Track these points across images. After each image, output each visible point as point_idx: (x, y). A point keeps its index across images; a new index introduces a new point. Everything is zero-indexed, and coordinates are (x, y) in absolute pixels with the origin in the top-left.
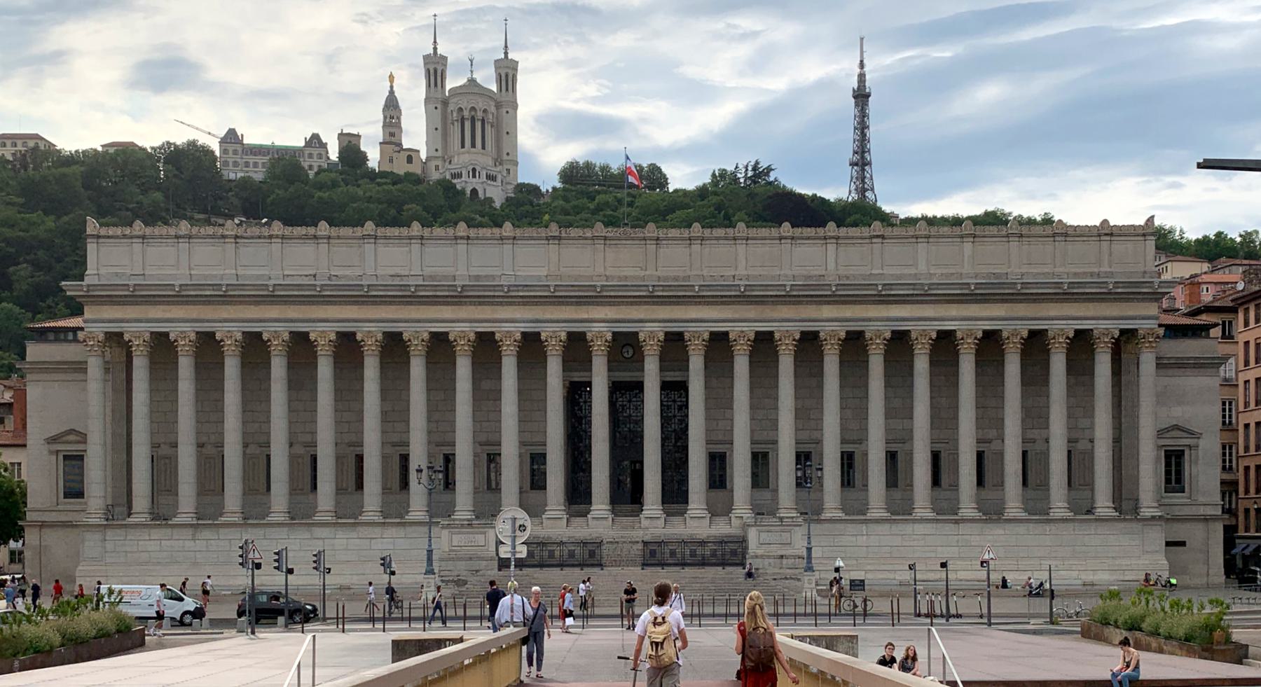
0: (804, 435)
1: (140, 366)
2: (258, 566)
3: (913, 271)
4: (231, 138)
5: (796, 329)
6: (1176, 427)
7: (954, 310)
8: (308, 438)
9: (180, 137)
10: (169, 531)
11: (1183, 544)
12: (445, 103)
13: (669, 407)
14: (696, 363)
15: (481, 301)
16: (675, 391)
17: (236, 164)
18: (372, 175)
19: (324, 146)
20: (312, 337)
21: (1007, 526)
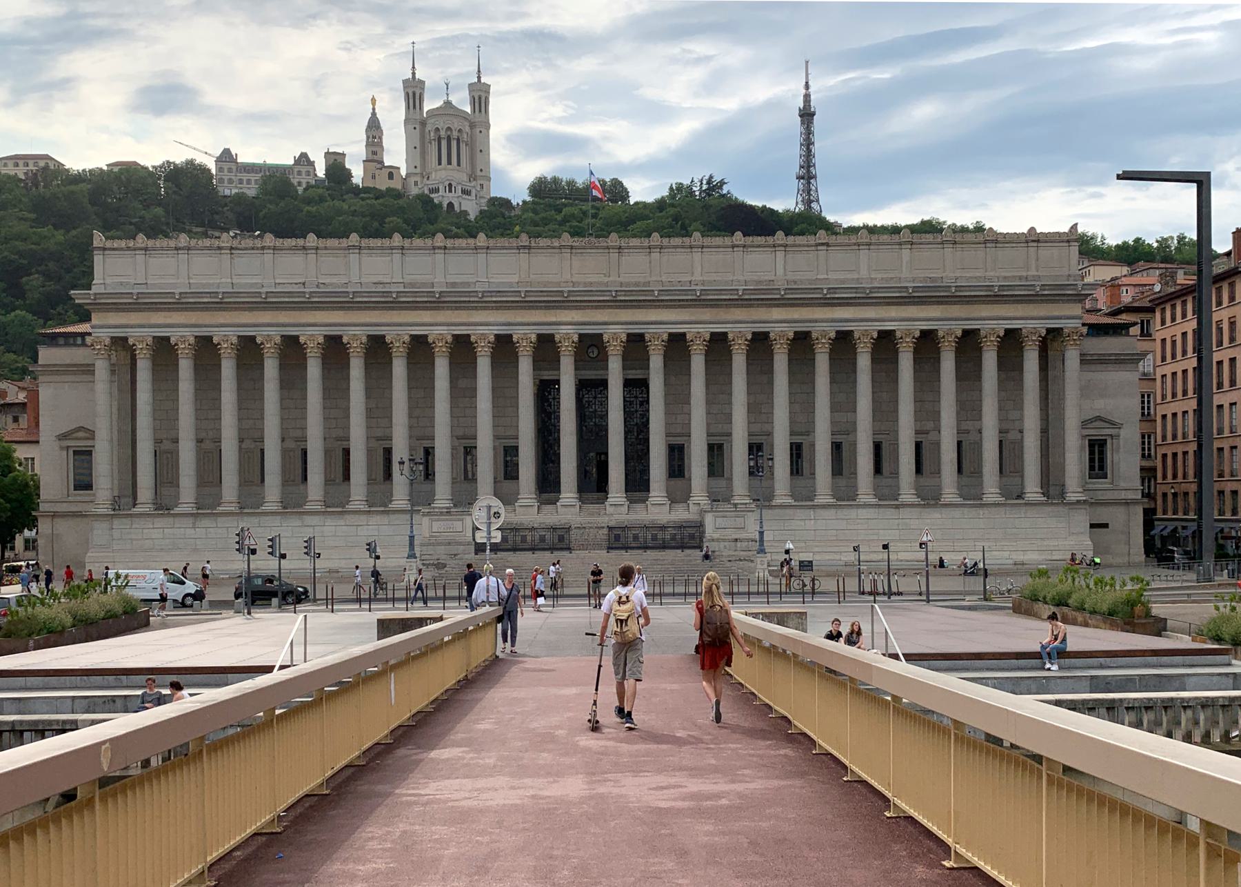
0: (756, 428)
2: (254, 552)
3: (856, 276)
4: (226, 157)
5: (748, 330)
6: (1099, 418)
7: (894, 312)
8: (298, 433)
10: (171, 519)
11: (1106, 526)
12: (423, 123)
13: (631, 403)
14: (656, 362)
15: (458, 306)
16: (637, 388)
17: (230, 181)
18: (356, 191)
19: (312, 164)
21: (944, 510)
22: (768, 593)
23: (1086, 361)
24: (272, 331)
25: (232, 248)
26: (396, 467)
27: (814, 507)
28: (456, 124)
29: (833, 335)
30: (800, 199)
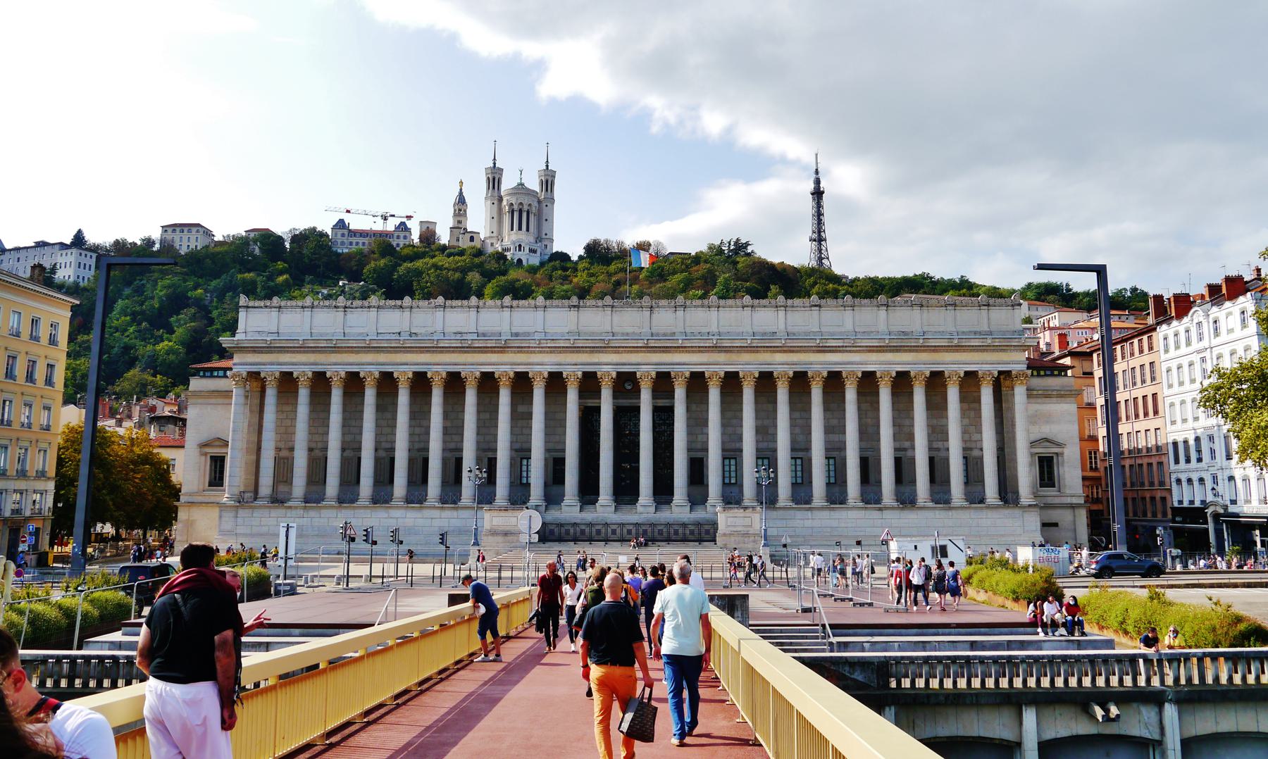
1: (271, 394)
2: (353, 540)
4: (341, 224)
7: (874, 357)
8: (388, 446)
9: (302, 225)
14: (680, 393)
16: (663, 417)
17: (343, 243)
18: (443, 248)
20: (395, 375)
21: (920, 512)
22: (383, 577)
23: (1031, 394)
26: (465, 474)
27: (810, 509)
28: (526, 201)
29: (825, 374)
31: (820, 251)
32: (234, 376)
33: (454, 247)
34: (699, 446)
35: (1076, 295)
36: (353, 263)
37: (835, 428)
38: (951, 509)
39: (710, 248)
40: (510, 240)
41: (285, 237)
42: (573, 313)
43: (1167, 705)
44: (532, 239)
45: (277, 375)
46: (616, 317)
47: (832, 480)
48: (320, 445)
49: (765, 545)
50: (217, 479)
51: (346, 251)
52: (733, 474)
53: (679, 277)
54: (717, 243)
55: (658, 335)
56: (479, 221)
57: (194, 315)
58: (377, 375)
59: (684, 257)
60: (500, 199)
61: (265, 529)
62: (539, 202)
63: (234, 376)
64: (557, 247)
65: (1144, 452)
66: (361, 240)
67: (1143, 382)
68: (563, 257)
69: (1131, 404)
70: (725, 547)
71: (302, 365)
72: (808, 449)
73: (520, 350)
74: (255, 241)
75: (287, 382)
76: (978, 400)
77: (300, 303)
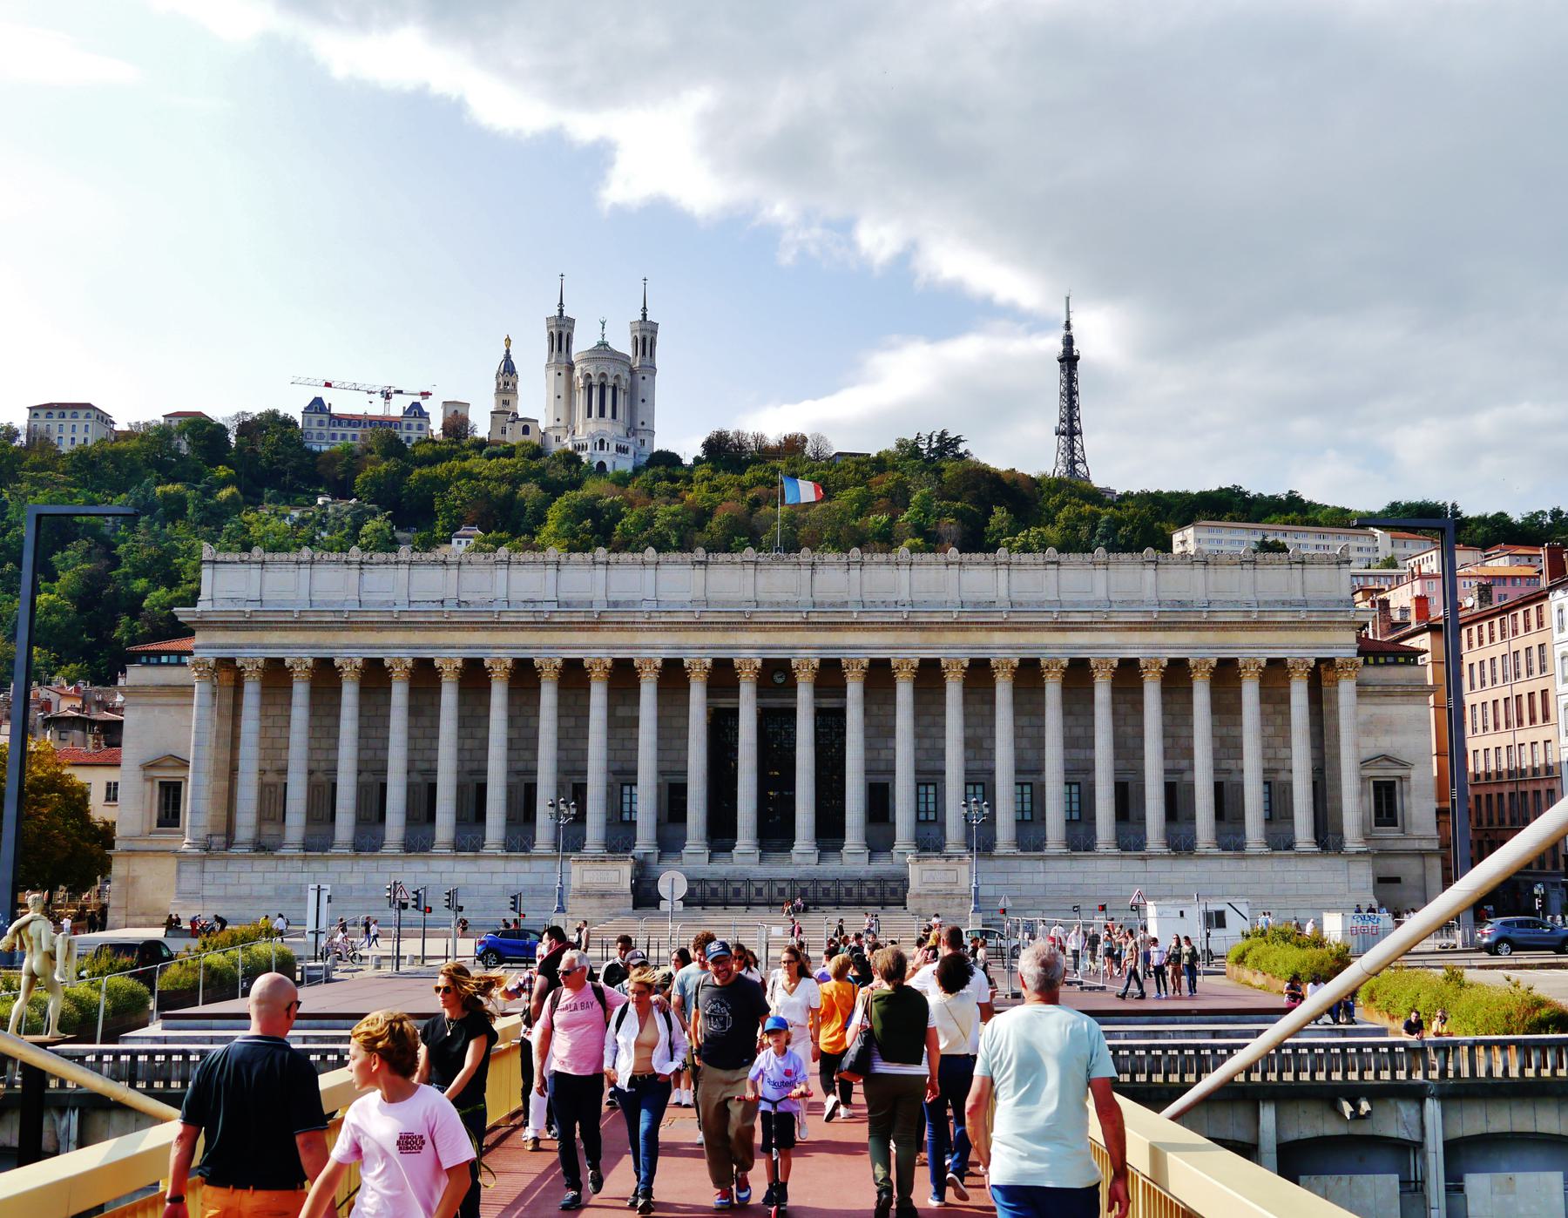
0: (976, 765)
2: (405, 906)
4: (317, 406)
6: (1386, 758)
7: (1137, 637)
8: (425, 766)
9: (256, 408)
10: (273, 863)
14: (854, 691)
16: (830, 725)
18: (481, 445)
20: (437, 664)
21: (1199, 862)
22: (424, 958)
23: (1363, 690)
24: (402, 653)
25: (362, 563)
27: (1043, 858)
29: (1065, 663)
30: (1060, 458)
31: (1072, 450)
32: (196, 665)
33: (497, 443)
34: (882, 767)
35: (1466, 522)
36: (338, 468)
37: (1078, 742)
38: (1244, 857)
39: (900, 446)
40: (586, 433)
41: (229, 427)
42: (699, 573)
43: (1428, 1101)
44: (621, 432)
45: (261, 663)
46: (762, 578)
47: (1075, 816)
48: (323, 765)
49: (976, 910)
50: (169, 815)
51: (325, 448)
52: (931, 807)
53: (853, 492)
54: (911, 437)
55: (822, 604)
56: (537, 401)
57: (88, 552)
58: (409, 663)
59: (860, 460)
60: (571, 367)
61: (245, 890)
62: (632, 372)
63: (196, 665)
64: (660, 444)
65: (1529, 775)
66: (350, 431)
67: (1530, 672)
68: (670, 459)
69: (1513, 703)
70: (919, 913)
71: (299, 649)
72: (1040, 770)
73: (621, 626)
74: (181, 433)
75: (276, 674)
76: (1286, 700)
77: (293, 556)
